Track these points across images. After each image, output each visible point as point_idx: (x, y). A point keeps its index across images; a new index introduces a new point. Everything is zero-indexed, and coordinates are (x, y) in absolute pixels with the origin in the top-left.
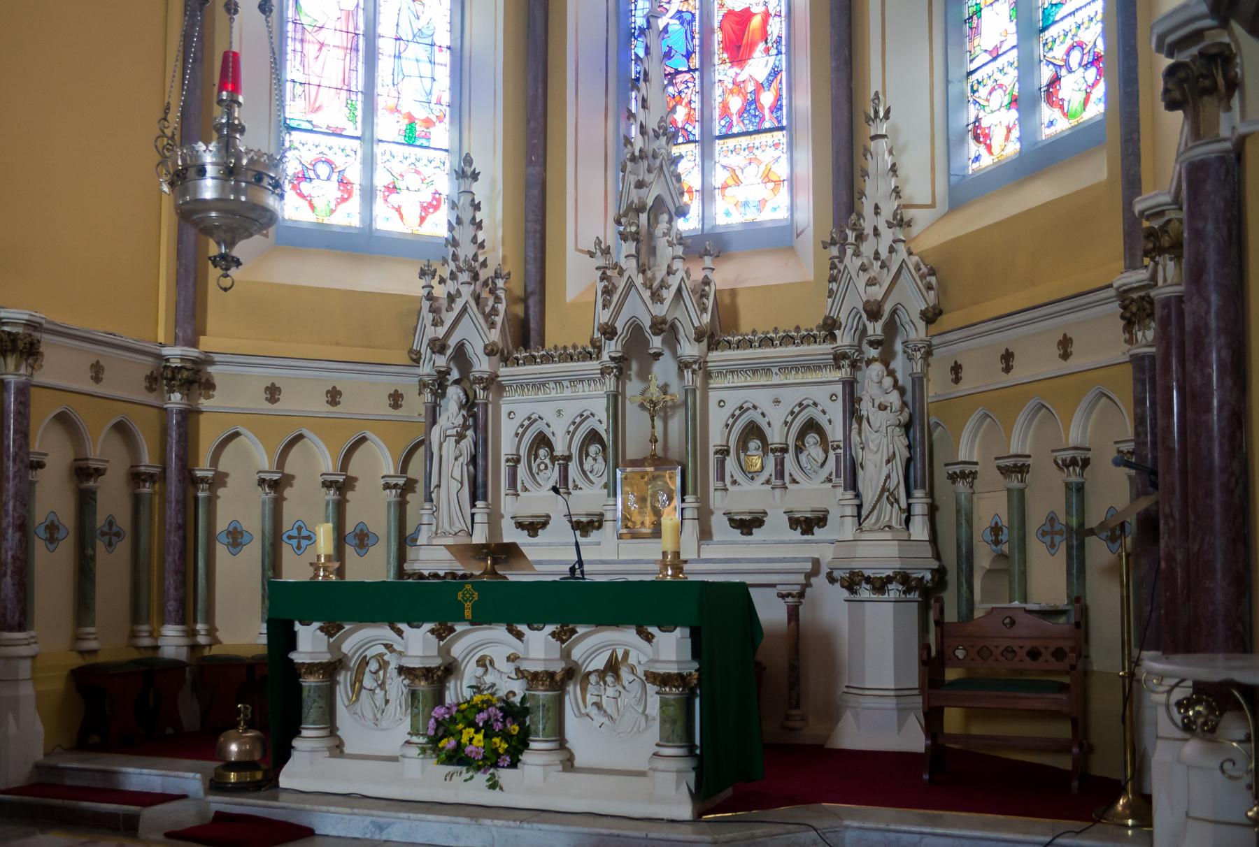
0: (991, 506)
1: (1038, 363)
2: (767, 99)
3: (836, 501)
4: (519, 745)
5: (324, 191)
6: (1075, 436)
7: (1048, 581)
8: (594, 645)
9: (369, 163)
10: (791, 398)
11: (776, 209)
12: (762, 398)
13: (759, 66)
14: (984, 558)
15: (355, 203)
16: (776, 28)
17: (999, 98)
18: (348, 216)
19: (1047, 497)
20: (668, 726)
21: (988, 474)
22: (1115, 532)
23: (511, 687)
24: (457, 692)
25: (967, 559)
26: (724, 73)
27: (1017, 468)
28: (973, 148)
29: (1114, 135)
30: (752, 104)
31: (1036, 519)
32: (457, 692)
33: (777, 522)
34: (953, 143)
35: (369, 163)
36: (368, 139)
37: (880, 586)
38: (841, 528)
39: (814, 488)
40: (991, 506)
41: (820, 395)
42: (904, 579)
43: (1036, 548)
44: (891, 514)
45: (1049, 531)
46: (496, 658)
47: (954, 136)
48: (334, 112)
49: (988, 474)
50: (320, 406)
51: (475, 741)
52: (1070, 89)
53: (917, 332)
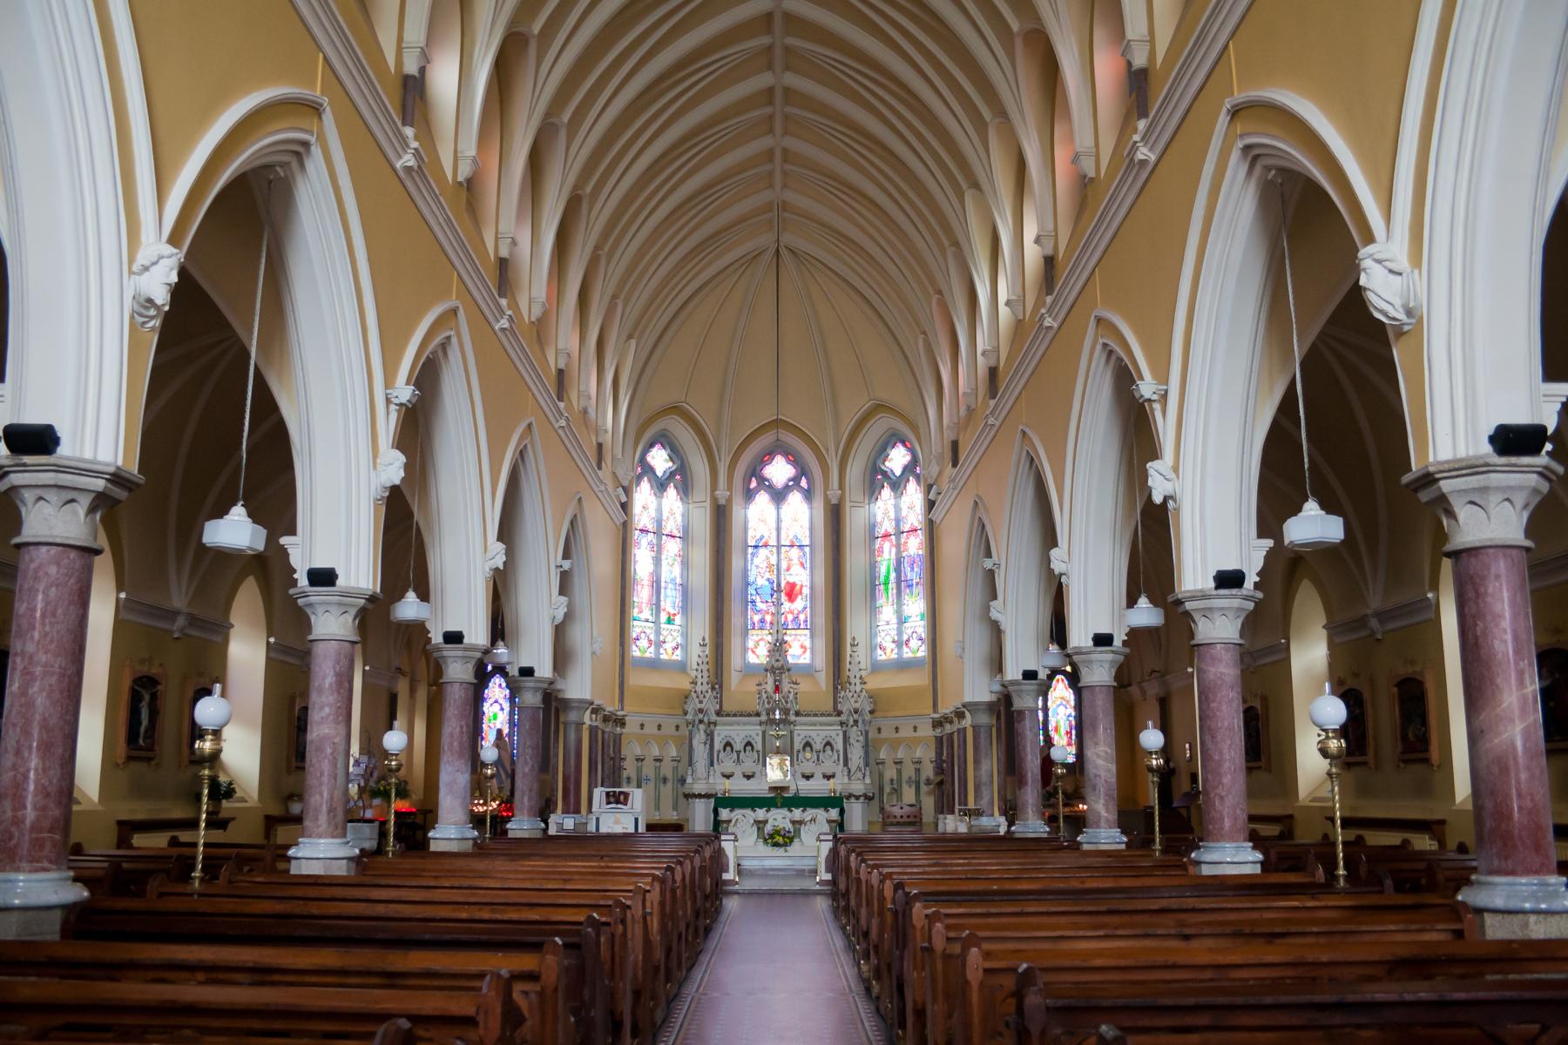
1: (906, 732)
2: (802, 617)
3: (839, 769)
4: (791, 840)
5: (643, 643)
7: (909, 795)
8: (810, 813)
9: (658, 633)
10: (823, 734)
11: (806, 659)
12: (813, 734)
13: (799, 604)
14: (887, 789)
15: (652, 649)
16: (806, 591)
17: (889, 639)
18: (650, 653)
19: (909, 771)
21: (889, 763)
22: (928, 782)
23: (789, 826)
24: (768, 828)
25: (881, 789)
26: (787, 606)
27: (898, 763)
28: (879, 652)
30: (796, 618)
31: (905, 777)
32: (768, 828)
33: (818, 775)
35: (658, 633)
36: (657, 622)
37: (857, 798)
39: (830, 763)
40: (890, 773)
41: (833, 734)
42: (865, 796)
43: (905, 786)
44: (859, 775)
45: (909, 781)
46: (779, 818)
48: (646, 614)
49: (889, 763)
50: (655, 731)
51: (779, 839)
52: (914, 643)
53: (868, 717)
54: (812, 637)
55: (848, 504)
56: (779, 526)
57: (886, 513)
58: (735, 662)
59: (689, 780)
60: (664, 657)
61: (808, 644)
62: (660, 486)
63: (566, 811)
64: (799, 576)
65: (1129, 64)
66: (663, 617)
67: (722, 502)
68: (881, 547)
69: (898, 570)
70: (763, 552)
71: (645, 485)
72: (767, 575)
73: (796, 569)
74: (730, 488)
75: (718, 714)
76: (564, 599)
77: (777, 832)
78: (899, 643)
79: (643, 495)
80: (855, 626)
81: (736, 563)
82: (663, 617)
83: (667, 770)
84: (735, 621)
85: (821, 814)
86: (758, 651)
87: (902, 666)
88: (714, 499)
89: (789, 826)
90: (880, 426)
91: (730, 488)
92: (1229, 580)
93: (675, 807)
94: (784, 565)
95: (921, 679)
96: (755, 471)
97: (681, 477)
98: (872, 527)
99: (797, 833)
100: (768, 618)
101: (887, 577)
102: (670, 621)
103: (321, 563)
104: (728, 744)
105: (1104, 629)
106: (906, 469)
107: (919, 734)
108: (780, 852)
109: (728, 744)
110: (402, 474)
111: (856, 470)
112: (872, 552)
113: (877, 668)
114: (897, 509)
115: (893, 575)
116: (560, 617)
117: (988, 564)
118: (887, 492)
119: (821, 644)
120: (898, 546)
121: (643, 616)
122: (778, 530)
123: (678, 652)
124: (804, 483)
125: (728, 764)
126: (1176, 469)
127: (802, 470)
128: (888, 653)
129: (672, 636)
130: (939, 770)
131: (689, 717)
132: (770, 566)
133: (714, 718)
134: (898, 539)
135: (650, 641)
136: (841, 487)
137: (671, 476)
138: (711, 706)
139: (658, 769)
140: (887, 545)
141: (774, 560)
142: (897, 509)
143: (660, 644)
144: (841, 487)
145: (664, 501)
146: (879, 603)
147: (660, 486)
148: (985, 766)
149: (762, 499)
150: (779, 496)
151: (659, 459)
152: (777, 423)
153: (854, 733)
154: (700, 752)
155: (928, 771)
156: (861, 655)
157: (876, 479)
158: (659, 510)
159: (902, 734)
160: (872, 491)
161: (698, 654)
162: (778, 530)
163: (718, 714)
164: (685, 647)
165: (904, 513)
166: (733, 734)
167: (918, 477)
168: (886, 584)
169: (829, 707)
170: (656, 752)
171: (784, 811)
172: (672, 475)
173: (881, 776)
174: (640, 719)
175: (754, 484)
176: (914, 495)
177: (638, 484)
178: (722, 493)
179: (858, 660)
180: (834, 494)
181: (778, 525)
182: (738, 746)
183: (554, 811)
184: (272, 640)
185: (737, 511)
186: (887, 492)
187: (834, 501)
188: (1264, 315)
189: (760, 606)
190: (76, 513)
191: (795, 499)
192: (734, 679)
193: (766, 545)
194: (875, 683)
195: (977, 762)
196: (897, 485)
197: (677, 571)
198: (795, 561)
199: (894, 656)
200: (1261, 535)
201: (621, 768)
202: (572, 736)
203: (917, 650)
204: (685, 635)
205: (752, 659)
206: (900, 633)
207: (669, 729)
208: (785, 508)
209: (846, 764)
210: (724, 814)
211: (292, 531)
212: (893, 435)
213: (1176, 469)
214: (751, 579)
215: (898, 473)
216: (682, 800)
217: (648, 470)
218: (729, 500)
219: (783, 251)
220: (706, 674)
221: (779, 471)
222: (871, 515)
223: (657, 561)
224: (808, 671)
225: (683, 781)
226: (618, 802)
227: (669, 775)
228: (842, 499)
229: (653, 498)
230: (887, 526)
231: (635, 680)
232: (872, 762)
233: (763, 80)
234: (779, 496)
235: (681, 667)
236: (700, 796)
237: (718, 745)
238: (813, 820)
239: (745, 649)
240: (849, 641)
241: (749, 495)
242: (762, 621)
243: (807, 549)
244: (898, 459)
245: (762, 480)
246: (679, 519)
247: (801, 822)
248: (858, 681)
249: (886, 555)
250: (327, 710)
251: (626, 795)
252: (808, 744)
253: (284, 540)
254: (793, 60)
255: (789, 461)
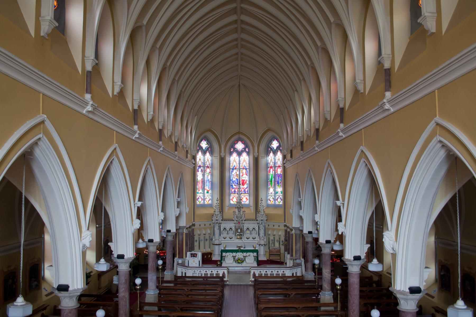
0: (272, 238)
1: (276, 227)
2: (246, 190)
4: (243, 262)
5: (200, 200)
6: (280, 234)
7: (277, 245)
8: (248, 254)
9: (204, 196)
10: (252, 226)
11: (247, 202)
13: (245, 186)
14: (271, 242)
16: (248, 182)
18: (202, 202)
19: (277, 238)
20: (375, 278)
23: (242, 257)
24: (237, 258)
29: (283, 206)
31: (276, 240)
32: (237, 258)
34: (267, 201)
35: (204, 196)
36: (204, 193)
37: (262, 245)
38: (257, 239)
39: (254, 234)
40: (272, 238)
42: (265, 245)
44: (263, 238)
45: (277, 241)
47: (267, 200)
48: (201, 191)
50: (204, 226)
51: (240, 261)
52: (279, 200)
54: (249, 196)
55: (260, 157)
56: (240, 161)
57: (271, 160)
58: (227, 204)
59: (214, 240)
60: (206, 203)
61: (248, 198)
62: (204, 153)
63: (179, 258)
64: (245, 178)
65: (339, 105)
66: (206, 191)
67: (223, 156)
68: (270, 170)
69: (275, 177)
70: (235, 171)
71: (200, 153)
72: (236, 177)
73: (245, 176)
74: (225, 152)
75: (222, 220)
76: (178, 209)
77: (239, 259)
78: (275, 200)
79: (200, 155)
80: (262, 195)
81: (227, 174)
82: (206, 191)
83: (207, 237)
84: (227, 191)
85: (251, 254)
86: (234, 201)
87: (276, 206)
88: (220, 156)
89: (242, 257)
90: (270, 134)
91: (225, 152)
92: (357, 258)
93: (210, 248)
94: (241, 174)
95: (281, 212)
96: (233, 146)
97: (210, 150)
98: (267, 164)
99: (245, 260)
100: (236, 190)
101: (271, 179)
102: (208, 192)
103: (120, 253)
104: (225, 229)
105: (329, 239)
106: (277, 148)
107: (280, 228)
108: (240, 265)
109: (225, 229)
110: (140, 226)
111: (262, 147)
112: (267, 172)
113: (268, 206)
114: (275, 159)
115: (273, 179)
116: (177, 215)
117: (300, 199)
118: (271, 154)
119: (252, 198)
120: (275, 171)
121: (200, 192)
122: (239, 164)
123: (210, 201)
124: (247, 150)
125: (225, 234)
126: (345, 226)
127: (246, 146)
128: (271, 202)
129: (208, 197)
130: (286, 240)
131: (213, 221)
132: (237, 175)
133: (221, 222)
134: (275, 169)
135: (202, 199)
136: (258, 152)
137: (207, 149)
138: (220, 218)
139: (205, 237)
140: (271, 170)
141: (238, 173)
142: (275, 159)
143: (204, 200)
144: (258, 152)
145: (206, 157)
146: (269, 187)
147: (204, 153)
148: (298, 246)
149: (235, 155)
150: (239, 154)
151: (204, 144)
152: (239, 133)
153: (261, 226)
154: (217, 232)
155: (283, 238)
156: (264, 203)
157: (268, 150)
158: (204, 160)
159: (275, 227)
160: (267, 154)
161: (216, 203)
162: (239, 164)
163: (222, 220)
164: (212, 200)
165: (277, 161)
166: (226, 226)
167: (281, 151)
168: (271, 181)
169: (255, 218)
170: (204, 232)
171: (241, 253)
172: (208, 149)
173: (269, 238)
174: (199, 223)
175: (232, 150)
176: (279, 156)
177: (198, 153)
178: (223, 154)
179: (263, 204)
180: (256, 154)
181: (240, 161)
182: (228, 229)
183: (176, 257)
184: (97, 226)
185: (227, 158)
186: (271, 154)
187: (256, 156)
188: (369, 193)
189: (234, 187)
190: (73, 300)
191: (244, 155)
192: (226, 209)
193: (236, 169)
194: (268, 211)
195: (296, 244)
196: (275, 153)
197: (209, 177)
198: (244, 173)
199: (273, 203)
200: (367, 243)
201: (194, 238)
202: (181, 237)
203: (280, 202)
204: (212, 196)
205: (232, 202)
206: (275, 197)
207: (208, 225)
208: (241, 158)
209: (259, 235)
210: (224, 254)
211: (111, 241)
212: (274, 137)
213: (345, 226)
214: (231, 179)
215: (275, 149)
216: (212, 245)
217: (201, 148)
218: (225, 156)
219: (241, 85)
220: (218, 209)
221: (240, 146)
222: (267, 161)
223: (204, 175)
224: (248, 206)
225: (212, 239)
226: (194, 257)
227: (208, 238)
228: (258, 156)
229: (202, 156)
230: (272, 164)
231: (199, 212)
232: (266, 234)
233: (234, 18)
234: (239, 154)
235: (210, 206)
236: (217, 245)
237: (222, 229)
238: (249, 255)
239: (230, 200)
240: (260, 199)
241: (231, 154)
242: (235, 191)
243: (248, 170)
244: (275, 144)
245: (235, 149)
246: (210, 162)
247: (245, 257)
248: (263, 211)
249: (271, 173)
250: (123, 289)
251: (196, 254)
252: (248, 229)
253: (109, 244)
254: (243, 30)
255: (242, 143)
